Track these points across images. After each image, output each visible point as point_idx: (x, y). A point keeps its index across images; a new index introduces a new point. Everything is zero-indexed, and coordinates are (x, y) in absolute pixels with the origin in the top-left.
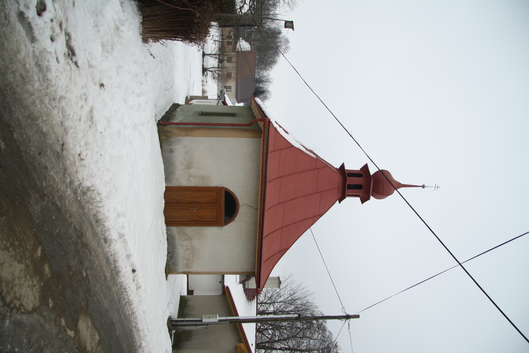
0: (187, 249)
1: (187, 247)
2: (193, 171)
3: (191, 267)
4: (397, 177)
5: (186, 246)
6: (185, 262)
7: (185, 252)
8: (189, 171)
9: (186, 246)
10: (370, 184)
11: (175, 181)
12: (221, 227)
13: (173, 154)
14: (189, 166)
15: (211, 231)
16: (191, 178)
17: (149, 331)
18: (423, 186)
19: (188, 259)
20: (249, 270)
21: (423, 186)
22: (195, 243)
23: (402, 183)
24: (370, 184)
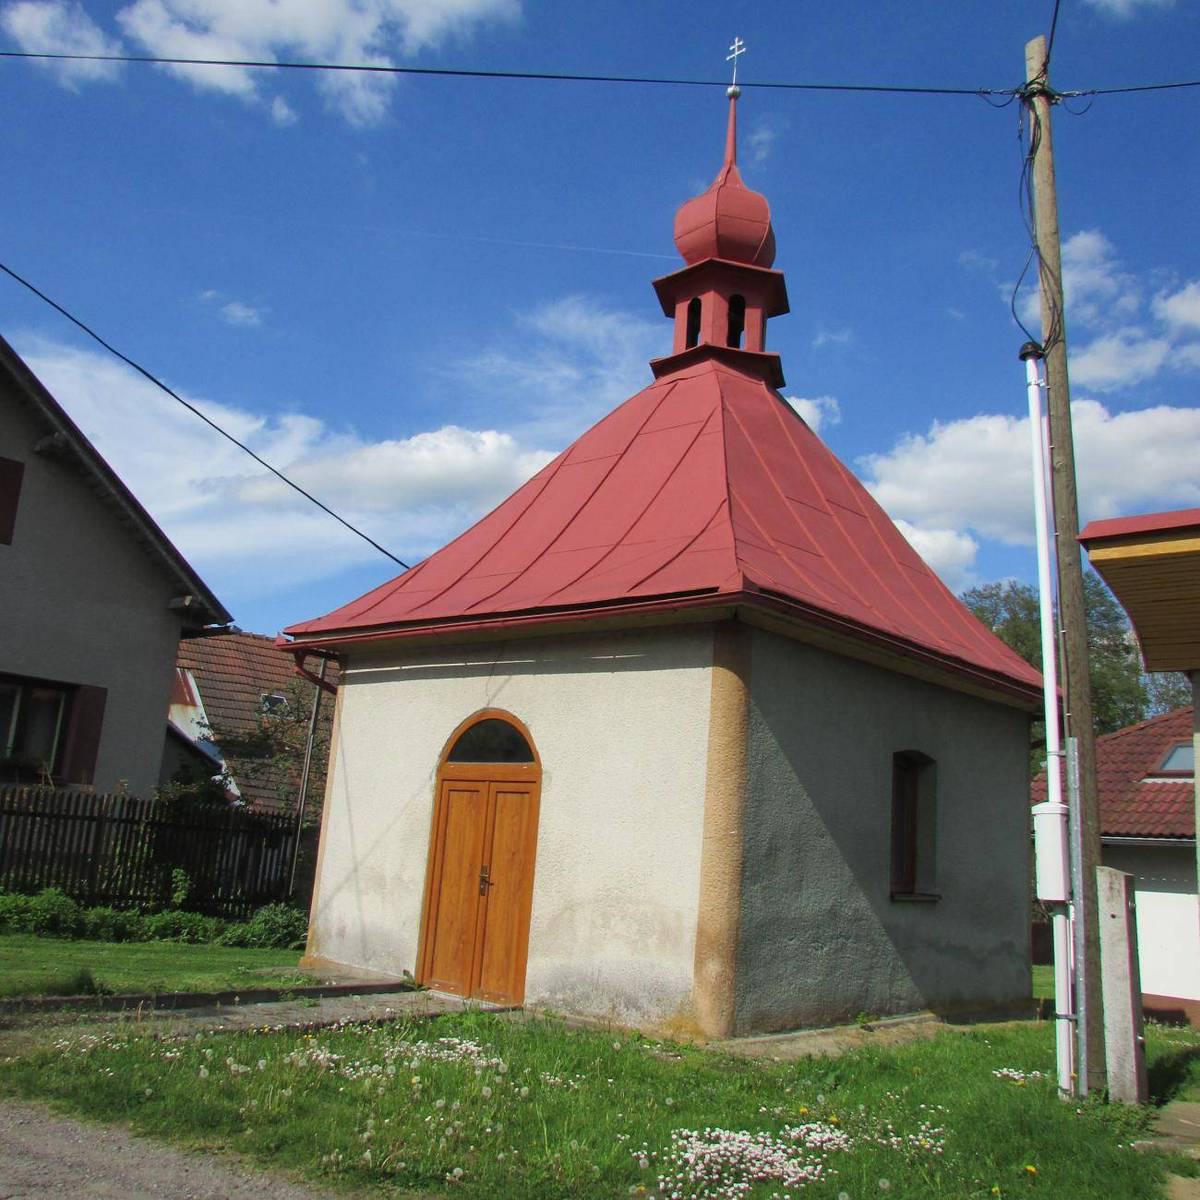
12: (544, 776)
16: (405, 878)
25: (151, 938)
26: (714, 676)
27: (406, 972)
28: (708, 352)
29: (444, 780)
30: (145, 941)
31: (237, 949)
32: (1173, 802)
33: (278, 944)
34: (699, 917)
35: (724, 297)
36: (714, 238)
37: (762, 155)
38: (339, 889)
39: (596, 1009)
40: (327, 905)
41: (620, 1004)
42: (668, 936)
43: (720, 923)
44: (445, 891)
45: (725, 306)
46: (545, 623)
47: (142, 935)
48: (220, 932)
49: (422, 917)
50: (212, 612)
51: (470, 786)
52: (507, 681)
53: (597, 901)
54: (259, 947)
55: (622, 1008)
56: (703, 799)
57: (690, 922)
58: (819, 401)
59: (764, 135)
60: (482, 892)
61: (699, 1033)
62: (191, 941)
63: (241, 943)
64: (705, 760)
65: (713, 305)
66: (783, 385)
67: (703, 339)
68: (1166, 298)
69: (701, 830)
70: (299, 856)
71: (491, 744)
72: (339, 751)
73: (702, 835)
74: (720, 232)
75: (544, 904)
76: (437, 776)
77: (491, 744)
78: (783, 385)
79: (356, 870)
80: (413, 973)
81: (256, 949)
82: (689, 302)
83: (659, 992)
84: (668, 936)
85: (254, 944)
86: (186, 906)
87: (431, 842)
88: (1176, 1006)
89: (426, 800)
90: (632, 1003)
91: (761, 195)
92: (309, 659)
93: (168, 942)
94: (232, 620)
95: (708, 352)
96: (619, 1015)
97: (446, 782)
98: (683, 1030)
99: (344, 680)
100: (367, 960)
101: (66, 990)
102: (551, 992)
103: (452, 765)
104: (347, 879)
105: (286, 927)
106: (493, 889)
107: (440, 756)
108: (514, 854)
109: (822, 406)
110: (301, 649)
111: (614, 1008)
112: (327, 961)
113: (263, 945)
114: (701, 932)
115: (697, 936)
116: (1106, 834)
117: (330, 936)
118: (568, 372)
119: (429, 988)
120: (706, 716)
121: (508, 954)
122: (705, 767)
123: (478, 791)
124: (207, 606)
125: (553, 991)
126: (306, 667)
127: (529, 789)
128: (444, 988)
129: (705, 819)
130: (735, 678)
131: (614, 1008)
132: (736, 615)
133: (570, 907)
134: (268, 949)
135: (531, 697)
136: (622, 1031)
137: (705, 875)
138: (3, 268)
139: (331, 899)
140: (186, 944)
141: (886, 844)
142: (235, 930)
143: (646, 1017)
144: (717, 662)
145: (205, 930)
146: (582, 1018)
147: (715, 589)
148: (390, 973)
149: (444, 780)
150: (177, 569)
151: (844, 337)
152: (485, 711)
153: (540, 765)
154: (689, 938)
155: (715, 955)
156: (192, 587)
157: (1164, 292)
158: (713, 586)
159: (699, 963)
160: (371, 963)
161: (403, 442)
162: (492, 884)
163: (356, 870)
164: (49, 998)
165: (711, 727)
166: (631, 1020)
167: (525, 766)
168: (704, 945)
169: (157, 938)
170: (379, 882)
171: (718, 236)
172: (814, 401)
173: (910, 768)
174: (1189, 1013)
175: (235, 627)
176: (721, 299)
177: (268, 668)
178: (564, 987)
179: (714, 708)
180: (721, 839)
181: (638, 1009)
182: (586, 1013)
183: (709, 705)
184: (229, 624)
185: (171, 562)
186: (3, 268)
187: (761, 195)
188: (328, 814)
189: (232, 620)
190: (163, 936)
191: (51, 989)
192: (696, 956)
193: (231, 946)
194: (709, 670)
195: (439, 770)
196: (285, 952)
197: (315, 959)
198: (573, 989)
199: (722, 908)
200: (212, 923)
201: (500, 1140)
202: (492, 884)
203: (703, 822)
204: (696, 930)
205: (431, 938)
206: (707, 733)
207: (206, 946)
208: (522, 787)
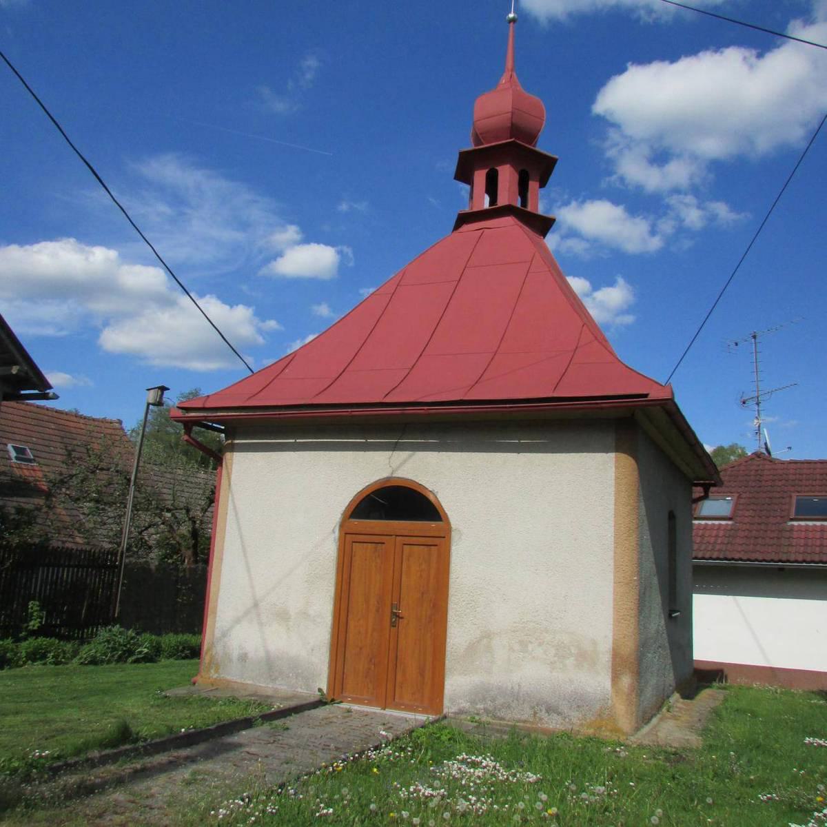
12: (453, 534)
25: (25, 663)
26: (617, 461)
27: (320, 690)
28: (508, 210)
29: (346, 534)
30: (21, 666)
31: (92, 667)
32: (717, 536)
33: (121, 659)
34: (613, 644)
35: (516, 171)
36: (510, 125)
37: (309, 76)
38: (238, 621)
39: (520, 714)
40: (224, 634)
41: (541, 710)
42: (584, 658)
43: (629, 647)
44: (352, 624)
45: (516, 177)
46: (487, 412)
47: (18, 660)
48: (75, 653)
50: (35, 379)
51: (377, 541)
52: (410, 456)
53: (514, 631)
54: (107, 664)
55: (543, 714)
56: (612, 554)
58: (340, 248)
59: (312, 62)
60: (393, 625)
61: (616, 730)
62: (57, 663)
63: (94, 662)
64: (612, 523)
65: (507, 175)
67: (502, 201)
68: (560, 207)
70: (123, 584)
71: (397, 506)
72: (230, 507)
73: (613, 581)
74: (514, 122)
76: (340, 530)
77: (397, 506)
79: (256, 605)
80: (325, 691)
81: (105, 666)
82: (487, 170)
83: (579, 701)
85: (102, 662)
86: (42, 631)
87: (337, 584)
88: (719, 667)
89: (330, 549)
91: (535, 98)
92: (196, 429)
93: (37, 667)
95: (508, 210)
96: (541, 719)
97: (348, 536)
98: (604, 729)
99: (233, 448)
100: (274, 680)
101: (113, 743)
102: (471, 703)
103: (356, 521)
104: (247, 613)
105: (125, 646)
106: (402, 623)
107: (342, 515)
108: (423, 593)
109: (340, 253)
110: (191, 421)
111: (535, 713)
112: (229, 681)
113: (109, 662)
114: (616, 655)
115: (612, 658)
116: (696, 558)
117: (231, 660)
118: (163, 208)
119: (342, 702)
120: (612, 490)
121: (422, 673)
122: (612, 529)
123: (384, 543)
124: (31, 374)
125: (473, 702)
127: (440, 544)
128: (356, 701)
129: (615, 569)
130: (633, 462)
131: (535, 713)
133: (488, 636)
134: (112, 665)
135: (434, 470)
136: (545, 732)
137: (617, 610)
138: (2, 55)
139: (232, 627)
140: (53, 666)
142: (87, 651)
143: (567, 720)
144: (617, 449)
145: (64, 652)
146: (505, 722)
147: (646, 396)
148: (299, 690)
149: (346, 534)
150: (12, 348)
151: (362, 207)
152: (388, 479)
153: (448, 524)
154: (605, 659)
155: (628, 670)
156: (18, 356)
157: (559, 203)
158: (645, 393)
159: (615, 678)
160: (277, 682)
161: (27, 247)
162: (402, 618)
163: (256, 605)
164: (103, 753)
166: (553, 723)
167: (433, 524)
168: (618, 665)
169: (30, 662)
170: (283, 616)
171: (512, 124)
172: (336, 248)
174: (726, 671)
175: (54, 394)
176: (514, 172)
177: (10, 423)
178: (484, 699)
179: (617, 484)
180: (627, 584)
181: (559, 714)
182: (507, 718)
183: (614, 482)
184: (48, 391)
185: (7, 341)
186: (2, 55)
187: (535, 98)
188: (222, 559)
190: (34, 660)
191: (102, 745)
192: (612, 673)
193: (86, 664)
194: (612, 455)
195: (342, 525)
196: (124, 666)
197: (215, 679)
198: (493, 700)
199: (631, 636)
200: (68, 647)
201: (312, 802)
202: (402, 618)
203: (612, 571)
204: (611, 653)
206: (613, 502)
207: (68, 666)
208: (429, 541)
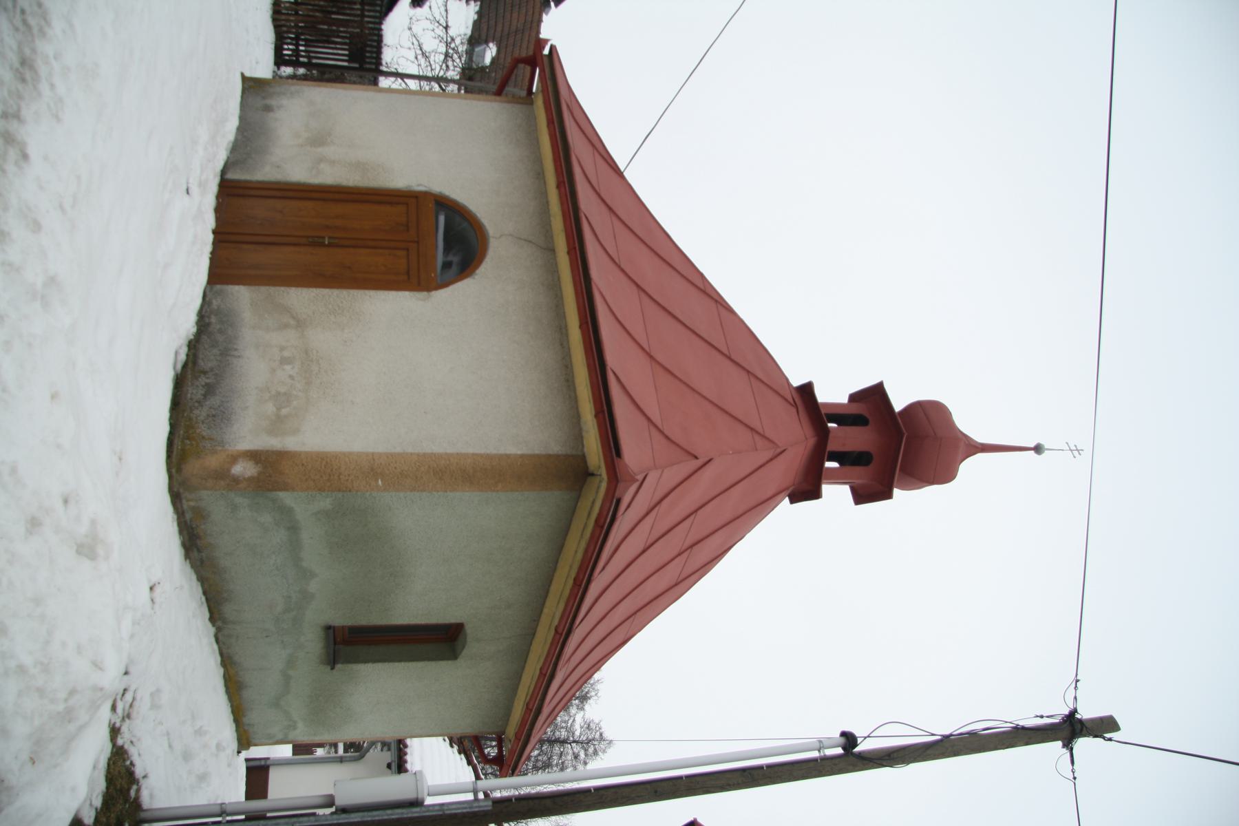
0: (284, 361)
1: (286, 354)
2: (329, 151)
3: (296, 431)
4: (967, 422)
5: (282, 349)
6: (270, 408)
7: (273, 371)
8: (320, 150)
9: (282, 349)
10: (890, 446)
11: (267, 169)
12: (425, 293)
13: (271, 114)
14: (319, 140)
15: (388, 309)
16: (322, 166)
17: (155, 706)
18: (1038, 449)
19: (282, 399)
20: (556, 448)
21: (1038, 449)
22: (323, 339)
23: (980, 437)
24: (890, 446)
42: (277, 424)
44: (310, 204)
49: (286, 184)
57: (291, 443)
66: (792, 502)
69: (381, 449)
75: (301, 298)
78: (792, 502)
84: (277, 424)
90: (210, 390)
94: (557, 5)
117: (264, 98)
126: (521, 66)
132: (592, 475)
141: (363, 621)
165: (481, 455)
173: (441, 640)
181: (205, 396)
189: (557, 5)
198: (221, 331)
205: (252, 192)
